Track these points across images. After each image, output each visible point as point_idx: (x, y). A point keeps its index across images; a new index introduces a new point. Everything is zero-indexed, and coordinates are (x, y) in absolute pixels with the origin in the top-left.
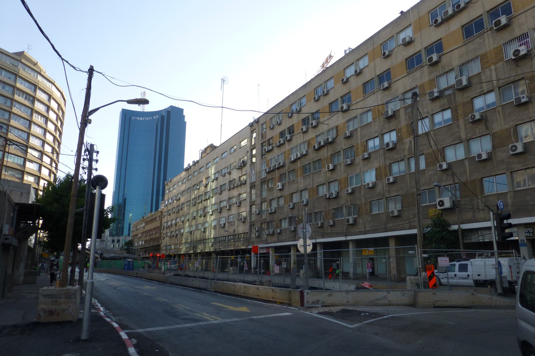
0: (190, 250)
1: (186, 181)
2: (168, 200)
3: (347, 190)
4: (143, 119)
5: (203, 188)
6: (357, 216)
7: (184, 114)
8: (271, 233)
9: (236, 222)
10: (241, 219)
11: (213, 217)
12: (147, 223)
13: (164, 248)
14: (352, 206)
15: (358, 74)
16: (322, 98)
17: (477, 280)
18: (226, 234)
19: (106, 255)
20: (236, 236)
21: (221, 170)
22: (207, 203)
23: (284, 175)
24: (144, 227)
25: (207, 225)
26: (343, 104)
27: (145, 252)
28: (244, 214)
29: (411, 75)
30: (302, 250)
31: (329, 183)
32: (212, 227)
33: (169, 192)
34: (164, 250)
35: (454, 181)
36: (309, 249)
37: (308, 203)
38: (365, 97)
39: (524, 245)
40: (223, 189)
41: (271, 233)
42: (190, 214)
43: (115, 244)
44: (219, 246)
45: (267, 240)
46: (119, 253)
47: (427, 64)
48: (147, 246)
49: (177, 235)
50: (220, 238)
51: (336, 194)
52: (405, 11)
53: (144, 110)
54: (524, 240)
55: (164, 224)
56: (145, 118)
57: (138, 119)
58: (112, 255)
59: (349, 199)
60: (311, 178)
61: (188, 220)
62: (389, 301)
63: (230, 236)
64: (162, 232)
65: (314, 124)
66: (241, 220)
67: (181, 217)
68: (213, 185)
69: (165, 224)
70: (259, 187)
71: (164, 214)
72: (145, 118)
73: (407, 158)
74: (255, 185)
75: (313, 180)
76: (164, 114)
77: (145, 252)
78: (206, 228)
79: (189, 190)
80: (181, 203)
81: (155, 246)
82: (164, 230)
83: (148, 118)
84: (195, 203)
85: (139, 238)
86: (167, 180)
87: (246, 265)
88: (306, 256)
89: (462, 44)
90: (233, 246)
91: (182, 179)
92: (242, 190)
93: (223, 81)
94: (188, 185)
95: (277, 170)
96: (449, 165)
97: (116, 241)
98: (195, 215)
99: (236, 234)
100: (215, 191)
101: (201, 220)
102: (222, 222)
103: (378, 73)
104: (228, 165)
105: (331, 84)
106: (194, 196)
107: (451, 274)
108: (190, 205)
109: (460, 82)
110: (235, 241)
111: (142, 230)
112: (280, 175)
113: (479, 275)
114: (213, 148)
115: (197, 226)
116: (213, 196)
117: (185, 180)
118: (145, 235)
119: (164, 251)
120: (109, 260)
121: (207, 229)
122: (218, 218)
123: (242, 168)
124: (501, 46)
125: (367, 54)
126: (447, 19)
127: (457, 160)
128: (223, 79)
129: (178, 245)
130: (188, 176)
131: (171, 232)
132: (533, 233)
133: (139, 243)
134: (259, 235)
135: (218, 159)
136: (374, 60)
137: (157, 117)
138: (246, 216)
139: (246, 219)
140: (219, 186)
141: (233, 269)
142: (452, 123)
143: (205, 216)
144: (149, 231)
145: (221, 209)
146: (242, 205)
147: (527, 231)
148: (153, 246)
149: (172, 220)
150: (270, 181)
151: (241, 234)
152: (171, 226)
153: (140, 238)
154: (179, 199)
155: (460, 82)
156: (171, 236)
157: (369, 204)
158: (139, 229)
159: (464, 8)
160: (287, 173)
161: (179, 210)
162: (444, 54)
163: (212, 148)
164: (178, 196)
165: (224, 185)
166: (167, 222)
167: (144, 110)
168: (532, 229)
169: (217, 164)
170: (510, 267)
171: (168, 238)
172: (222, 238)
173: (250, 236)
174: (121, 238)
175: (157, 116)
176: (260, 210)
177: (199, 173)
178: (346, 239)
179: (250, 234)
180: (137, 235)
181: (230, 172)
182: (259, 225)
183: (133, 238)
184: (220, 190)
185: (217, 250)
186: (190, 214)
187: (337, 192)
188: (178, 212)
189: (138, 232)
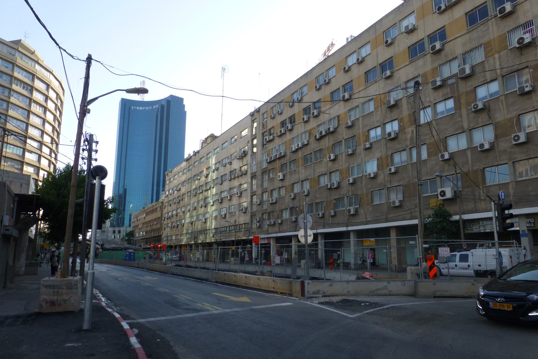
0: (191, 241)
2: (169, 191)
4: (143, 108)
5: (203, 179)
6: (358, 206)
8: (272, 223)
9: (237, 212)
10: (242, 210)
11: (214, 208)
12: (147, 214)
13: (165, 239)
15: (360, 62)
16: (323, 87)
19: (107, 246)
20: (237, 227)
21: (222, 160)
22: (208, 194)
25: (208, 216)
26: (345, 93)
27: (146, 243)
28: (245, 204)
29: (413, 64)
30: (302, 240)
31: (330, 173)
32: (213, 218)
33: (170, 182)
35: (456, 171)
36: (310, 239)
37: (309, 193)
39: (526, 235)
41: (272, 223)
42: (191, 205)
44: (220, 236)
45: (268, 231)
49: (178, 225)
50: (221, 229)
53: (143, 99)
54: (525, 230)
57: (138, 108)
58: (114, 246)
60: (312, 168)
61: (189, 211)
63: (231, 227)
64: (163, 223)
67: (187, 205)
68: (213, 175)
69: (166, 215)
70: (260, 177)
73: (409, 147)
75: (314, 170)
76: (164, 103)
77: (146, 243)
78: (207, 218)
80: (182, 194)
81: (156, 237)
82: (164, 220)
83: (148, 108)
84: (196, 193)
88: (306, 246)
89: (465, 32)
92: (242, 180)
93: (224, 69)
94: (189, 175)
95: (278, 160)
97: (117, 232)
98: (196, 206)
100: (216, 182)
104: (229, 155)
105: (332, 73)
106: (195, 187)
107: (452, 264)
109: (463, 70)
110: (237, 232)
111: (143, 221)
113: (480, 265)
115: (198, 216)
118: (146, 226)
119: (165, 242)
120: (110, 251)
121: (208, 219)
124: (505, 34)
125: (369, 42)
129: (179, 236)
130: (189, 166)
131: (172, 222)
132: (534, 223)
133: (140, 234)
134: (260, 225)
135: (218, 149)
136: (377, 48)
139: (247, 210)
140: (219, 176)
142: (454, 112)
145: (222, 200)
146: (243, 196)
147: (528, 222)
149: (173, 211)
150: (271, 171)
152: (172, 216)
154: (180, 190)
155: (463, 70)
156: (172, 227)
157: (370, 195)
161: (180, 201)
163: (213, 137)
166: (168, 213)
169: (218, 154)
170: (511, 257)
171: (169, 228)
172: (223, 228)
174: (122, 229)
176: (261, 200)
177: (200, 163)
178: (347, 229)
179: (251, 225)
180: (138, 226)
181: (231, 162)
182: (260, 215)
183: (134, 229)
184: (221, 180)
185: (218, 241)
188: (179, 203)
189: (139, 223)
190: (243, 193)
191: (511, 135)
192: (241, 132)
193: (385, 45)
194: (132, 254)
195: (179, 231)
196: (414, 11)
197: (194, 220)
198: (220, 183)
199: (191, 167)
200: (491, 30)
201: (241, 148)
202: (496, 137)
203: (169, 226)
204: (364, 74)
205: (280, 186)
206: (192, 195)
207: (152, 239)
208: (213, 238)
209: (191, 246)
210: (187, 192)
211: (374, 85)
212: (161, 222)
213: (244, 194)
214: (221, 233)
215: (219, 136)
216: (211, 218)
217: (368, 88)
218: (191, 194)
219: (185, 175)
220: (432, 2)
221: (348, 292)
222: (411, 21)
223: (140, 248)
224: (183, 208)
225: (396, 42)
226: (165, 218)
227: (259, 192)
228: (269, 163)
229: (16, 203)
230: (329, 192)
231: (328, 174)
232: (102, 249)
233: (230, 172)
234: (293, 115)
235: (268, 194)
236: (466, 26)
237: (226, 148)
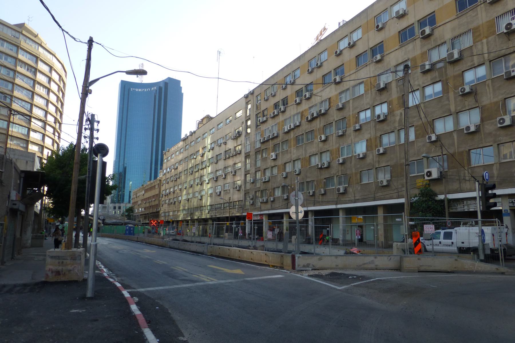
0: (187, 217)
2: (166, 169)
4: (141, 90)
5: (199, 158)
6: (347, 185)
7: (181, 86)
8: (265, 201)
9: (231, 190)
10: (236, 188)
11: (209, 186)
12: (146, 191)
14: (343, 176)
15: (351, 46)
16: (315, 70)
17: (461, 247)
18: (222, 201)
19: (108, 221)
20: (231, 204)
21: (217, 140)
23: (278, 145)
24: (144, 195)
25: (203, 193)
26: (336, 76)
27: (145, 218)
28: (239, 183)
29: (403, 48)
30: (294, 216)
31: (321, 153)
32: (209, 195)
33: (168, 161)
35: (442, 153)
36: (301, 216)
37: (300, 172)
38: (358, 69)
39: (508, 215)
41: (265, 201)
42: (188, 183)
45: (260, 208)
48: (146, 213)
49: (175, 202)
54: (507, 210)
57: (137, 90)
58: (114, 221)
59: (340, 170)
61: (186, 189)
62: (376, 265)
63: (225, 204)
64: (161, 200)
66: (236, 188)
68: (209, 155)
69: (164, 192)
70: (254, 157)
75: (306, 150)
76: (162, 85)
77: (145, 218)
78: (203, 196)
79: (187, 159)
80: (179, 172)
81: (154, 213)
82: (162, 197)
85: (139, 205)
89: (455, 17)
91: (179, 149)
92: (237, 159)
95: (270, 140)
97: (117, 208)
98: (192, 183)
100: (211, 161)
102: (218, 190)
106: (191, 165)
108: (187, 174)
110: (231, 209)
111: (142, 198)
112: (274, 145)
113: (463, 243)
115: (194, 193)
118: (145, 202)
121: (204, 196)
124: (493, 19)
125: (361, 26)
130: (186, 146)
133: (139, 210)
134: (253, 203)
135: (214, 130)
140: (215, 155)
142: (442, 95)
144: (148, 198)
145: (217, 178)
147: (511, 202)
148: (152, 213)
149: (170, 188)
150: (264, 151)
151: (236, 201)
152: (170, 193)
154: (177, 168)
155: (451, 55)
156: (169, 203)
157: (359, 175)
161: (177, 179)
166: (166, 190)
170: (493, 235)
171: (166, 205)
172: (218, 205)
174: (122, 205)
176: (255, 178)
177: (196, 143)
178: (336, 207)
179: (245, 202)
180: (137, 202)
181: (226, 142)
182: (254, 193)
184: (216, 159)
185: (213, 217)
186: (188, 183)
188: (176, 180)
189: (138, 199)
190: (237, 172)
193: (376, 29)
194: (132, 229)
198: (216, 162)
199: (187, 146)
203: (166, 202)
207: (151, 215)
209: (187, 221)
212: (159, 199)
215: (214, 117)
216: (206, 195)
218: (187, 172)
219: (182, 155)
224: (180, 185)
225: (387, 27)
226: (163, 195)
227: (253, 171)
228: (263, 143)
229: (22, 179)
230: (320, 171)
234: (301, 89)
235: (261, 173)
237: (222, 129)
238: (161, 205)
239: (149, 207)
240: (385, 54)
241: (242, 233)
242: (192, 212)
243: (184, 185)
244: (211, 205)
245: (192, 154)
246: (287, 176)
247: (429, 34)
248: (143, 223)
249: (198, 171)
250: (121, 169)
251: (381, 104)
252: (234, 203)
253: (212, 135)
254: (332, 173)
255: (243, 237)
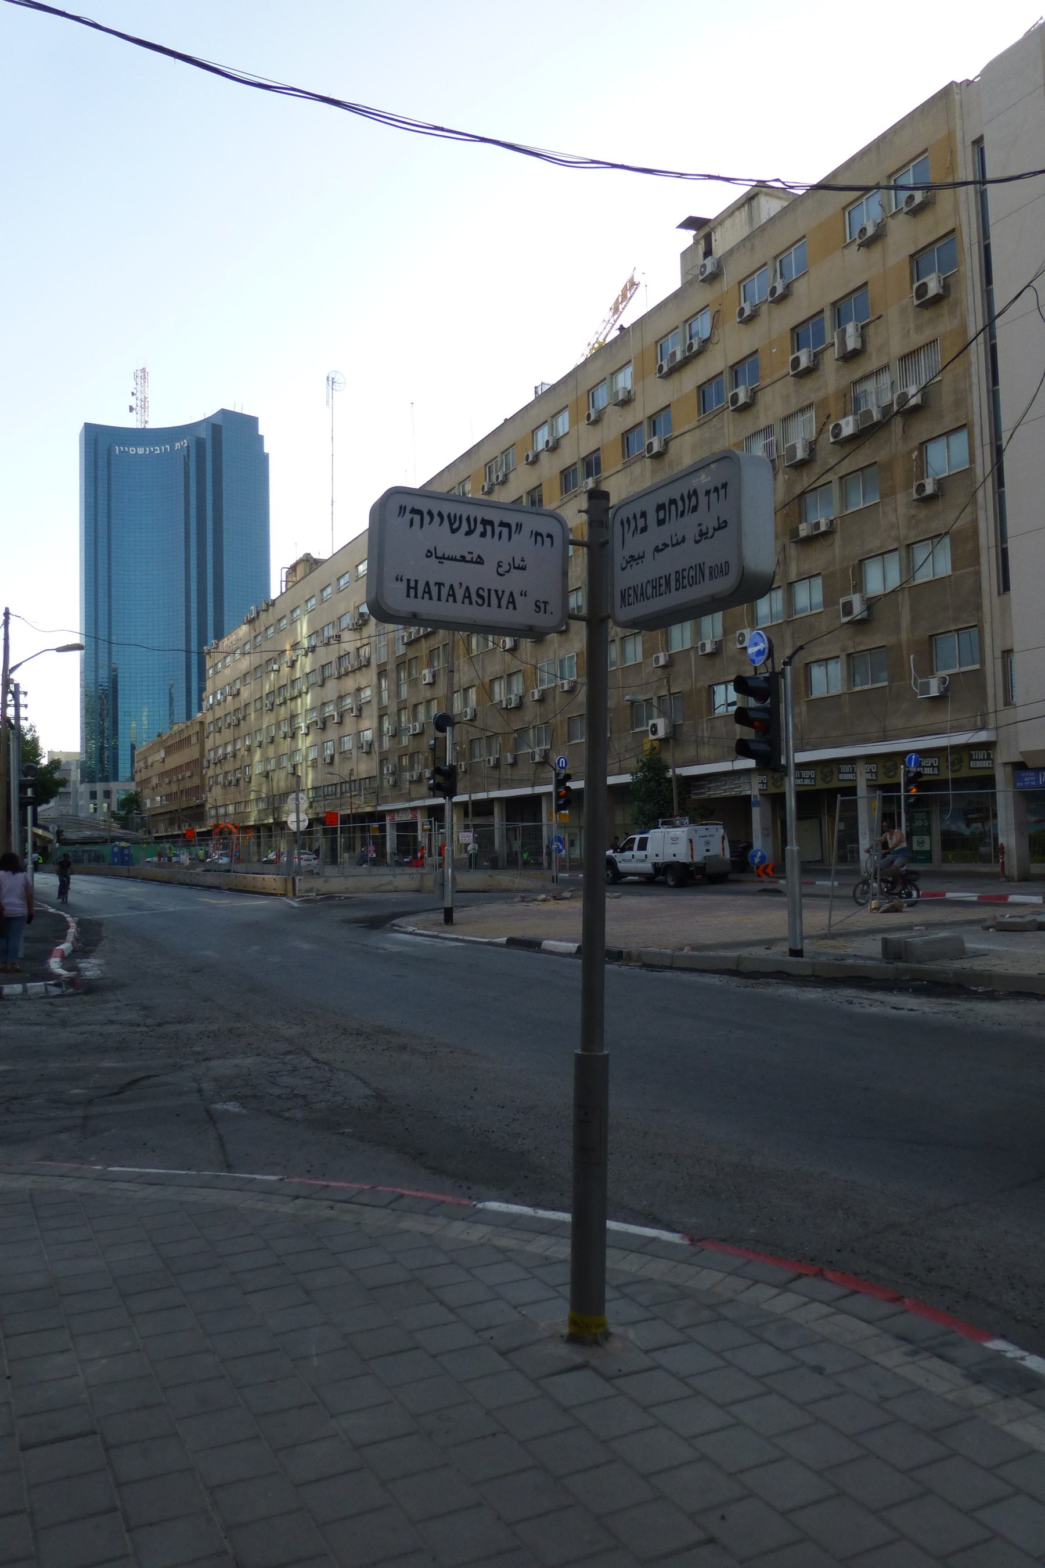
1: (250, 649)
2: (214, 695)
3: (657, 659)
4: (145, 450)
5: (285, 669)
6: (548, 747)
7: (260, 433)
9: (354, 752)
10: (362, 747)
11: (309, 740)
12: (169, 750)
13: (213, 812)
15: (553, 447)
16: (496, 488)
17: (655, 863)
18: (336, 780)
19: (70, 835)
20: (353, 783)
21: (323, 629)
22: (296, 705)
23: (437, 651)
24: (163, 761)
25: (298, 758)
26: (737, 387)
27: (171, 823)
28: (368, 735)
29: (628, 469)
30: (293, 827)
31: (510, 676)
32: (309, 763)
33: (216, 673)
34: (212, 817)
39: (758, 804)
40: (327, 674)
41: (415, 778)
42: (264, 731)
43: (98, 801)
46: (102, 827)
47: (789, 374)
49: (238, 780)
50: (326, 789)
51: (518, 700)
52: (680, 286)
53: (146, 422)
55: (209, 754)
56: (152, 449)
57: (132, 451)
58: (87, 833)
59: (538, 713)
61: (260, 746)
63: (344, 785)
64: (206, 774)
65: (742, 399)
66: (362, 749)
67: (245, 736)
68: (305, 664)
69: (212, 753)
70: (394, 675)
71: (207, 727)
72: (152, 449)
73: (620, 637)
74: (385, 670)
76: (204, 434)
77: (171, 823)
79: (259, 671)
80: (243, 704)
81: (191, 807)
82: (208, 767)
84: (272, 704)
85: (153, 789)
86: (209, 643)
87: (373, 847)
88: (298, 834)
90: (350, 807)
92: (368, 677)
93: (331, 381)
94: (255, 659)
95: (423, 639)
96: (871, 604)
97: (100, 795)
98: (273, 734)
99: (355, 778)
100: (312, 679)
101: (285, 746)
102: (328, 752)
103: (583, 455)
105: (563, 424)
107: (628, 854)
108: (262, 708)
110: (354, 796)
111: (159, 768)
112: (431, 651)
113: (675, 855)
114: (311, 564)
115: (279, 758)
116: (308, 691)
117: (247, 647)
118: (167, 780)
119: (212, 820)
121: (299, 767)
122: (319, 742)
123: (361, 629)
125: (567, 406)
126: (676, 369)
127: (936, 577)
128: (331, 379)
130: (255, 637)
131: (226, 773)
132: (876, 773)
133: (153, 802)
134: (395, 782)
135: (313, 601)
136: (578, 423)
137: (184, 443)
138: (372, 741)
140: (318, 666)
141: (349, 858)
142: (878, 501)
143: (293, 736)
144: (177, 769)
145: (324, 723)
146: (363, 715)
148: (187, 808)
149: (226, 744)
151: (365, 778)
152: (225, 758)
153: (157, 787)
154: (238, 693)
155: (904, 398)
156: (224, 784)
158: (152, 763)
159: (699, 353)
160: (441, 648)
161: (239, 721)
162: (673, 437)
164: (235, 685)
165: (328, 664)
166: (215, 749)
167: (146, 422)
168: (937, 759)
169: (313, 612)
170: (691, 841)
171: (219, 787)
172: (330, 788)
173: (382, 782)
174: (113, 786)
175: (185, 441)
180: (148, 780)
181: (339, 636)
182: (396, 759)
183: (139, 789)
184: (321, 678)
185: (320, 816)
186: (264, 731)
187: (520, 697)
188: (238, 725)
189: (151, 772)
190: (364, 709)
191: (735, 632)
192: (357, 566)
193: (658, 375)
194: (126, 851)
195: (242, 793)
196: (630, 361)
197: (272, 769)
199: (259, 639)
200: (726, 430)
201: (356, 605)
202: (726, 632)
203: (219, 780)
204: (908, 259)
205: (429, 698)
206: (265, 709)
207: (185, 813)
208: (310, 810)
209: (269, 827)
210: (253, 700)
211: (574, 501)
213: (366, 712)
214: (325, 797)
215: (327, 558)
216: (304, 763)
217: (564, 506)
219: (248, 658)
220: (657, 348)
221: (347, 888)
222: (625, 381)
223: (147, 836)
224: (247, 737)
225: (606, 418)
226: (209, 761)
227: (393, 709)
230: (507, 715)
231: (505, 677)
232: (58, 842)
233: (339, 658)
235: (409, 711)
236: (559, 493)
238: (207, 789)
239: (179, 794)
240: (602, 478)
241: (376, 851)
242: (276, 806)
243: (256, 739)
244: (316, 788)
245: (270, 659)
246: (396, 733)
247: (808, 367)
248: (156, 838)
249: (285, 703)
250: (103, 673)
251: (948, 434)
252: (360, 782)
253: (311, 613)
254: (526, 719)
255: (380, 860)
